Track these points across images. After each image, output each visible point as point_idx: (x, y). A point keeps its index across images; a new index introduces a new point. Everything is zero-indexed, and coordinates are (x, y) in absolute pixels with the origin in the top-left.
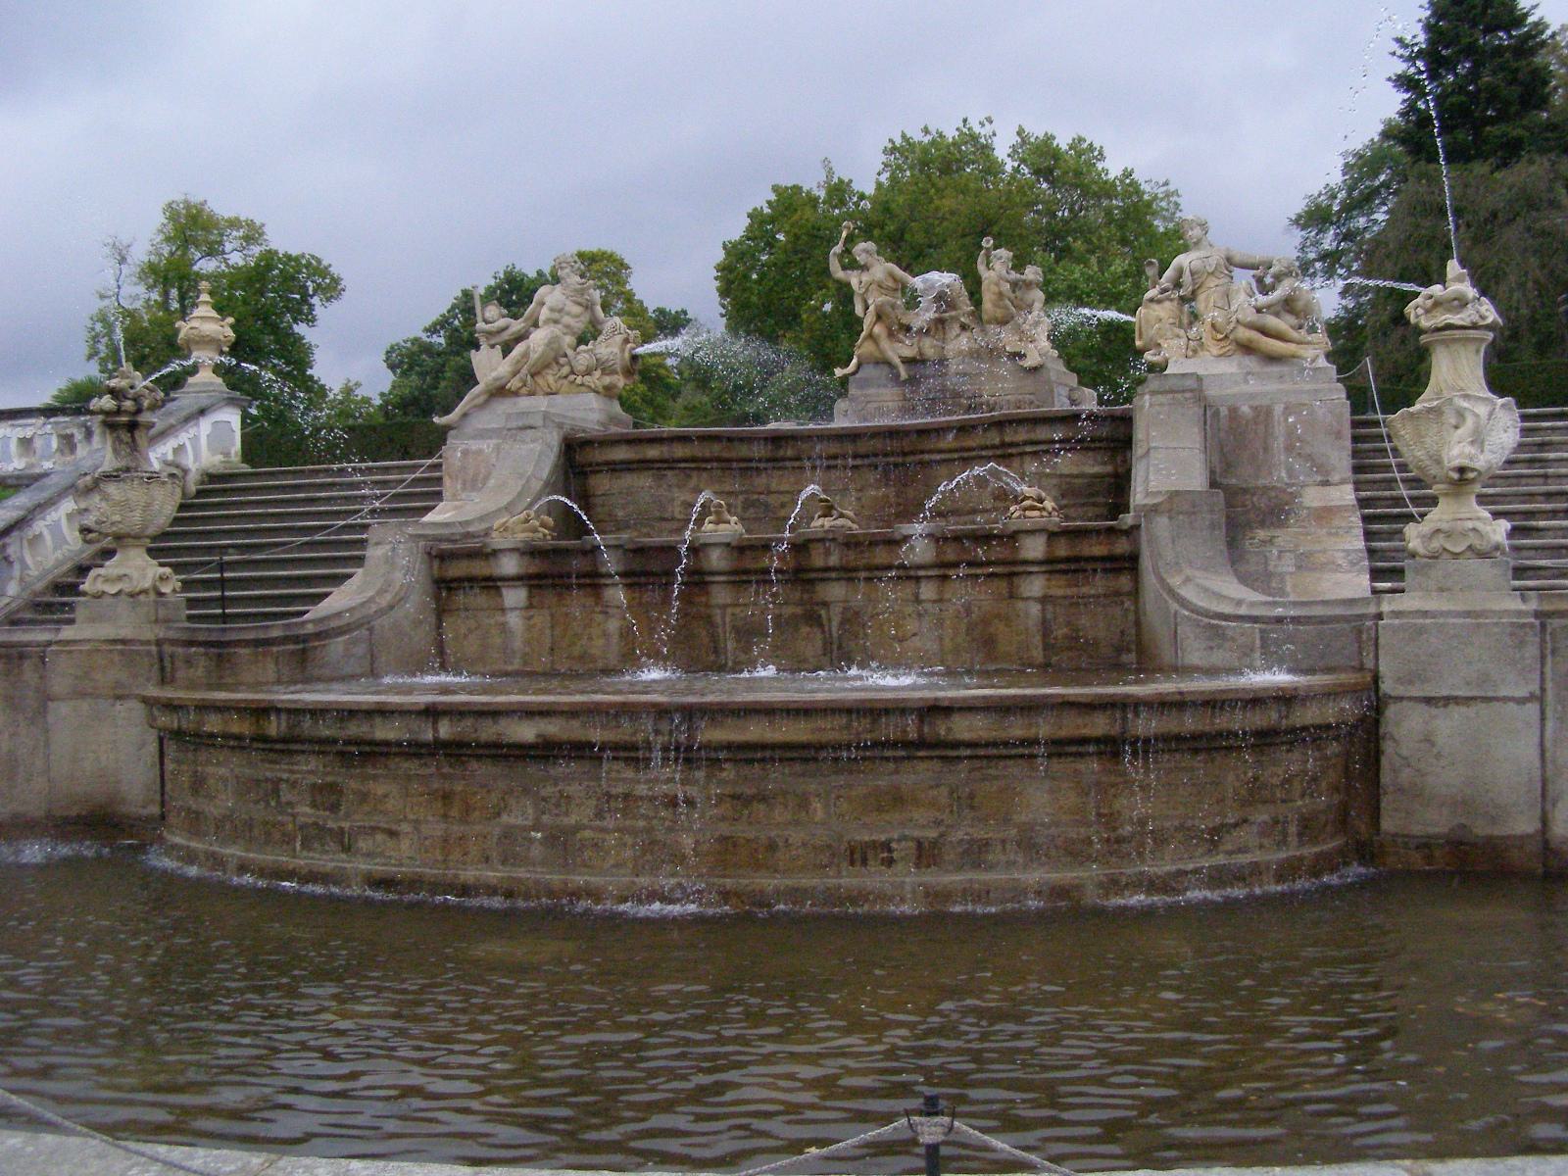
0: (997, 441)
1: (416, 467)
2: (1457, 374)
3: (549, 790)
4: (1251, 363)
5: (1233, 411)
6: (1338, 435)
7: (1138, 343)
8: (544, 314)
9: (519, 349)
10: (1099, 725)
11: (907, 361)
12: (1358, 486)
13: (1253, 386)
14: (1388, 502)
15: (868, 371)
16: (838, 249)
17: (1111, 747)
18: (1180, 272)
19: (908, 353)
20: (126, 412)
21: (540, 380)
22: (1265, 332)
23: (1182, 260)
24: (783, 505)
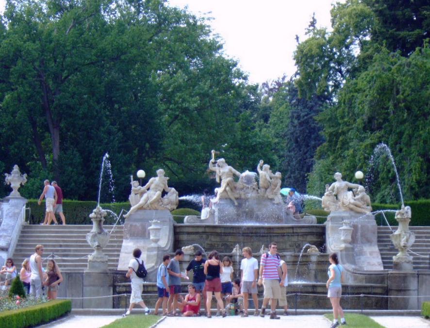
0: (292, 232)
1: (112, 227)
4: (353, 213)
6: (374, 233)
7: (323, 206)
8: (152, 186)
11: (237, 199)
12: (379, 246)
18: (334, 188)
19: (237, 196)
20: (98, 218)
21: (153, 205)
22: (356, 206)
24: (232, 245)
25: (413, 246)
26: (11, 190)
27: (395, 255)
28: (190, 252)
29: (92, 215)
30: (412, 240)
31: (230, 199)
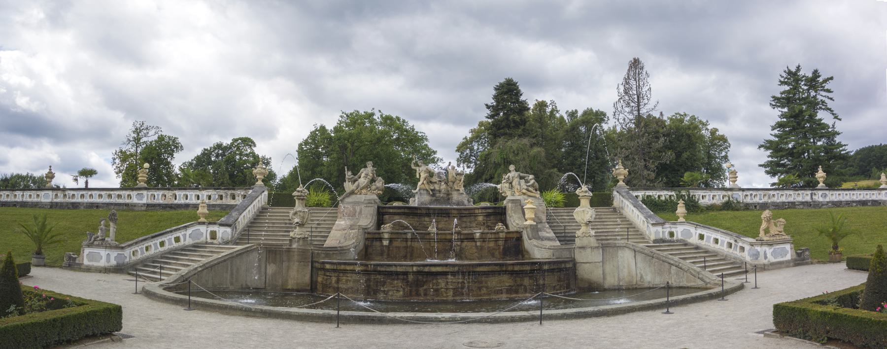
9: (356, 183)
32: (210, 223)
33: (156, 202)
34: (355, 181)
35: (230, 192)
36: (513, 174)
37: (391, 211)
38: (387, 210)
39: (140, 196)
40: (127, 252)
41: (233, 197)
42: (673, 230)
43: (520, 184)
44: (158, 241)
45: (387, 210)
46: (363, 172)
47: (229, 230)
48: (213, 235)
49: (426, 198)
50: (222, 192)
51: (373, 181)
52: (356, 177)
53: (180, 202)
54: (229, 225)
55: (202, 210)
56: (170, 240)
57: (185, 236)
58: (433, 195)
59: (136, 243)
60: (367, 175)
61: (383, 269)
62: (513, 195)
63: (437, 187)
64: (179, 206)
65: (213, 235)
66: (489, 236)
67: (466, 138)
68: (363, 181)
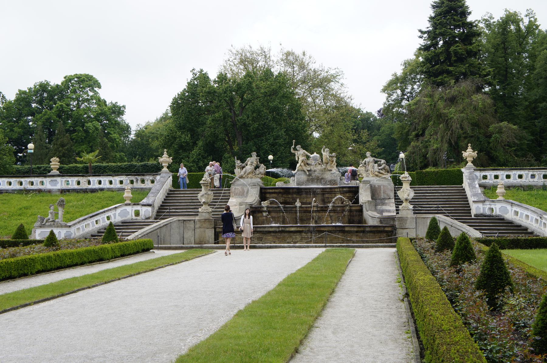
2: (406, 186)
3: (294, 237)
5: (375, 186)
9: (244, 169)
10: (362, 229)
11: (308, 171)
13: (378, 182)
14: (398, 202)
15: (300, 172)
16: (293, 146)
17: (363, 232)
19: (309, 169)
23: (365, 159)
25: (413, 199)
26: (163, 167)
27: (401, 205)
28: (266, 205)
29: (201, 182)
30: (412, 194)
31: (304, 171)
32: (134, 204)
33: (70, 187)
34: (243, 167)
35: (139, 178)
36: (369, 159)
37: (271, 191)
38: (268, 191)
39: (54, 183)
40: (73, 230)
41: (143, 181)
42: (493, 206)
43: (373, 167)
44: (94, 219)
45: (268, 191)
46: (249, 160)
47: (149, 209)
48: (137, 214)
49: (304, 177)
50: (133, 178)
51: (257, 167)
52: (244, 165)
53: (94, 187)
54: (149, 205)
55: (127, 194)
56: (103, 219)
57: (115, 215)
58: (310, 175)
59: (79, 222)
60: (252, 163)
61: (261, 230)
62: (367, 176)
63: (312, 168)
64: (93, 191)
65: (137, 214)
66: (354, 208)
67: (395, 75)
68: (249, 168)
